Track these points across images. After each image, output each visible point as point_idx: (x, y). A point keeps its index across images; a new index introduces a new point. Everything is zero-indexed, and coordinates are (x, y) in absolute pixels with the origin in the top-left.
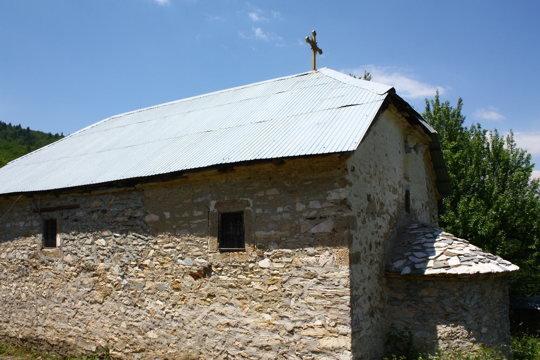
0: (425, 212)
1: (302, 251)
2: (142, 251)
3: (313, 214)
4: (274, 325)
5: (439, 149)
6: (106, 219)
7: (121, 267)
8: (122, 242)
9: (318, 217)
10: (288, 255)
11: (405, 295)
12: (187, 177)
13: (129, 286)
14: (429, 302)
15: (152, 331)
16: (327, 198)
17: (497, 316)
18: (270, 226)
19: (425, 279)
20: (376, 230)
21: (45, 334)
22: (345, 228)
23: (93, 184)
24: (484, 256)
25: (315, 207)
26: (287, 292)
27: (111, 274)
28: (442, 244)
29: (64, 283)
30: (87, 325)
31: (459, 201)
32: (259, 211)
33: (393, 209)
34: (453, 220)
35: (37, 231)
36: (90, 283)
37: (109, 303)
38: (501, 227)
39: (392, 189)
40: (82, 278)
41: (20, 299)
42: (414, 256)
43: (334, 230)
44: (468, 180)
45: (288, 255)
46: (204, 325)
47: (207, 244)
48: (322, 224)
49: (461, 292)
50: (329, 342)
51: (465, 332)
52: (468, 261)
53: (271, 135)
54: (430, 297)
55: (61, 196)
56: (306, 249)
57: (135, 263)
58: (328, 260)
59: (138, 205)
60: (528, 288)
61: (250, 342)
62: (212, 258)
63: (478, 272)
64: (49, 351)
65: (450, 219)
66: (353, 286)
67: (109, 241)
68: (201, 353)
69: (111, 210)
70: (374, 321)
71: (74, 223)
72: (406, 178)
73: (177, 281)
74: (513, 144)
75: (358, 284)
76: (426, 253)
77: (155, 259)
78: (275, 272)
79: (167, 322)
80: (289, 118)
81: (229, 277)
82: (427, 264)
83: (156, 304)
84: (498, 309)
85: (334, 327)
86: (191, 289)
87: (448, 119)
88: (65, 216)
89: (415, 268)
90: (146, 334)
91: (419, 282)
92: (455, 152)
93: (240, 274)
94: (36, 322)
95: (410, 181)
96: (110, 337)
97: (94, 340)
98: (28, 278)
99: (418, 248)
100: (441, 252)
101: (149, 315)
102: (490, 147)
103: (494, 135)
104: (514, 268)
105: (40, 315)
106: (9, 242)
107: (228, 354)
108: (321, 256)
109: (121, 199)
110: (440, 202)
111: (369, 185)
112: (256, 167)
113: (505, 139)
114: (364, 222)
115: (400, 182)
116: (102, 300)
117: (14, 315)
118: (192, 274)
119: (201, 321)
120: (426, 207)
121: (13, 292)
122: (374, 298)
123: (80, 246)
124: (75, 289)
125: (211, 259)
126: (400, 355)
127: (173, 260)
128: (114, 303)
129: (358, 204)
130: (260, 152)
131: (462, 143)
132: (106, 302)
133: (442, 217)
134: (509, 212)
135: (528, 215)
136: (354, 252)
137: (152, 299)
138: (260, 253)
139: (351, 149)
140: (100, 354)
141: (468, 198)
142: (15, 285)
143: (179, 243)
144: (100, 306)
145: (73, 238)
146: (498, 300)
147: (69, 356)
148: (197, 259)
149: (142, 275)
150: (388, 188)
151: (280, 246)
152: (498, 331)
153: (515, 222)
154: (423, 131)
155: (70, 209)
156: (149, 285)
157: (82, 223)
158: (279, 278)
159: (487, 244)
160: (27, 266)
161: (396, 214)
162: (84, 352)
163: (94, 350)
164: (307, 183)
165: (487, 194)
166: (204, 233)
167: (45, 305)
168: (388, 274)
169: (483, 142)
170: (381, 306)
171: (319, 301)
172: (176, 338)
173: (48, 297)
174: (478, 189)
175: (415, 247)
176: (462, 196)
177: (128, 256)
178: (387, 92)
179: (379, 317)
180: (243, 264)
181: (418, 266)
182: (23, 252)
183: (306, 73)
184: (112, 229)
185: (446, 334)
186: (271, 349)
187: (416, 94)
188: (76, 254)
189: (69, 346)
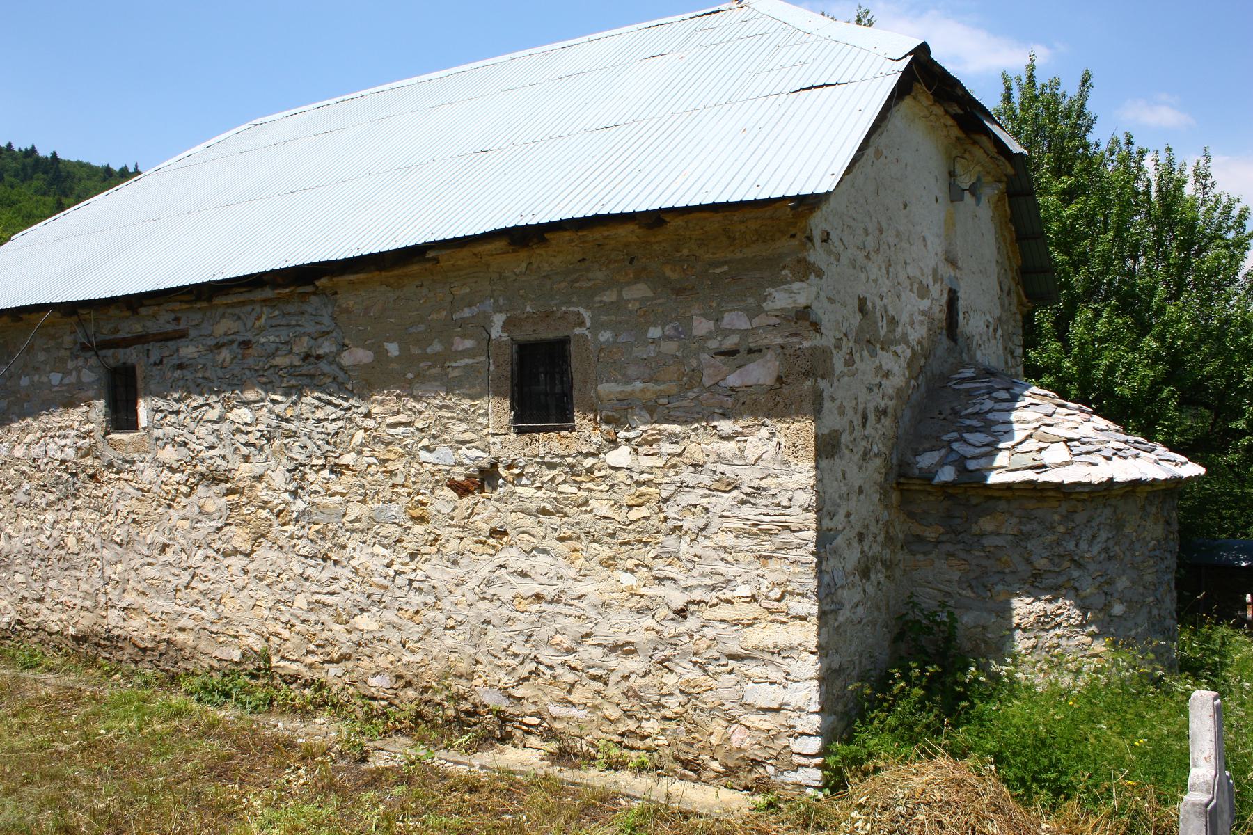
0: (993, 342)
1: (705, 428)
2: (337, 433)
3: (731, 342)
4: (642, 596)
5: (1030, 194)
6: (250, 361)
7: (289, 471)
8: (290, 413)
9: (743, 349)
10: (674, 439)
11: (942, 530)
12: (436, 260)
13: (310, 513)
14: (996, 547)
15: (365, 614)
16: (764, 305)
17: (1149, 578)
18: (632, 371)
19: (990, 493)
20: (878, 380)
21: (125, 624)
22: (807, 375)
23: (217, 281)
24: (1126, 442)
25: (737, 327)
26: (671, 523)
28: (1030, 415)
29: (161, 510)
30: (219, 603)
31: (1072, 317)
32: (605, 336)
33: (917, 333)
34: (1058, 362)
35: (91, 393)
36: (219, 509)
37: (264, 552)
38: (1168, 379)
39: (916, 286)
40: (200, 498)
41: (63, 548)
42: (966, 442)
43: (779, 379)
44: (1097, 266)
45: (674, 438)
46: (484, 599)
47: (486, 415)
48: (751, 366)
49: (1071, 525)
50: (766, 635)
51: (1076, 612)
52: (1090, 453)
53: (633, 157)
54: (999, 534)
55: (143, 311)
56: (715, 423)
57: (322, 462)
58: (765, 449)
59: (325, 329)
60: (1223, 518)
61: (589, 635)
62: (498, 446)
63: (1111, 480)
64: (136, 662)
65: (1050, 358)
66: (822, 509)
67: (259, 413)
68: (477, 662)
69: (262, 340)
71: (177, 373)
73: (419, 501)
74: (1209, 182)
75: (834, 504)
76: (992, 434)
77: (366, 451)
78: (645, 477)
79: (398, 593)
80: (676, 116)
81: (539, 488)
82: (993, 461)
83: (373, 555)
84: (1152, 562)
85: (779, 600)
86: (452, 519)
87: (1056, 121)
88: (154, 357)
89: (966, 470)
90: (352, 621)
91: (974, 501)
92: (1067, 203)
93: (565, 482)
94: (102, 599)
95: (960, 269)
96: (271, 629)
97: (235, 637)
98: (79, 502)
99: (975, 422)
100: (1028, 432)
101: (358, 579)
102: (1153, 189)
103: (1163, 159)
104: (1194, 469)
105: (112, 584)
106: (29, 420)
107: (539, 663)
108: (750, 439)
109: (284, 315)
110: (1028, 319)
111: (863, 276)
112: (597, 234)
113: (1189, 171)
114: (850, 362)
115: (935, 271)
116: (249, 547)
117: (52, 584)
118: (453, 485)
119: (477, 590)
120: (995, 330)
121: (48, 533)
122: (871, 538)
123: (192, 426)
124: (187, 524)
125: (495, 451)
126: (927, 663)
127: (409, 454)
128: (277, 554)
129: (836, 319)
130: (607, 199)
131: (1085, 180)
132: (260, 551)
133: (1033, 354)
134: (1188, 344)
135: (1235, 351)
136: (826, 431)
137: (364, 543)
138: (608, 433)
139: (821, 189)
140: (251, 667)
141: (1094, 309)
142: (50, 516)
143: (421, 413)
144: (246, 561)
145: (176, 407)
146: (1154, 542)
147: (182, 673)
148: (464, 450)
149: (339, 488)
150: (907, 283)
151: (655, 418)
152: (1150, 612)
153: (1202, 368)
154: (993, 150)
155: (167, 340)
156: (355, 510)
157: (196, 371)
158: (652, 490)
159: (1136, 417)
160: (74, 475)
161: (925, 343)
162: (215, 664)
163: (237, 659)
164: (718, 271)
165: (1140, 300)
166: (478, 389)
167: (120, 562)
168: (904, 483)
169: (1137, 178)
170: (887, 554)
171: (744, 543)
172: (421, 628)
173: (126, 544)
174: (1119, 288)
175: (968, 422)
176: (1081, 306)
177: (304, 447)
178: (910, 53)
179: (882, 580)
180: (570, 460)
181: (972, 465)
182: (63, 442)
183: (716, 9)
184: (265, 384)
185: (1032, 618)
186: (635, 651)
187: (982, 63)
188: (185, 444)
189: (181, 650)
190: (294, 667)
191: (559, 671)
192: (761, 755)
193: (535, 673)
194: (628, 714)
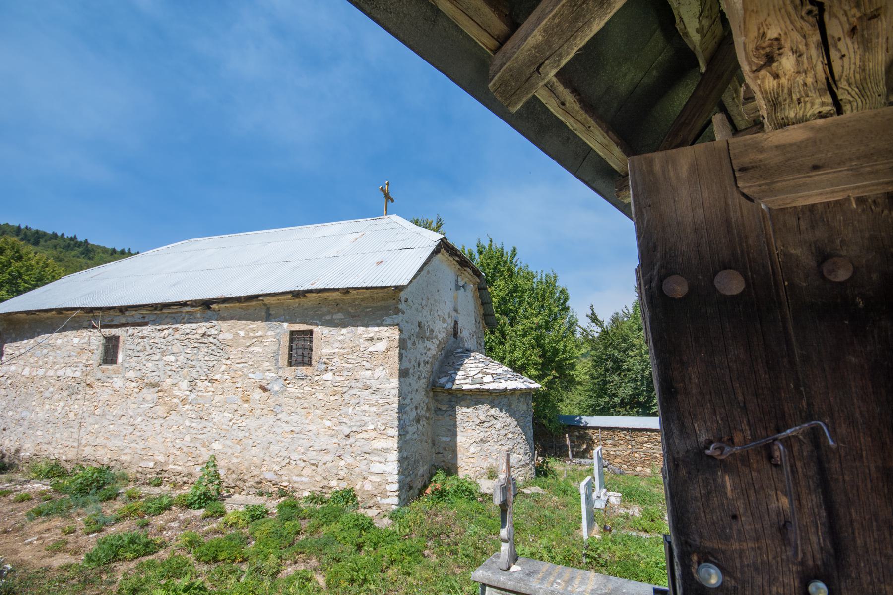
27: (179, 389)
33: (442, 336)
37: (173, 417)
50: (379, 444)
55: (127, 313)
70: (420, 428)
72: (456, 311)
98: (79, 397)
104: (536, 385)
114: (414, 344)
115: (449, 314)
123: (145, 363)
124: (135, 406)
132: (171, 417)
148: (267, 373)
156: (218, 398)
162: (140, 469)
170: (427, 415)
171: (373, 409)
190: (179, 468)
191: (299, 462)
192: (375, 492)
193: (289, 463)
194: (325, 479)
